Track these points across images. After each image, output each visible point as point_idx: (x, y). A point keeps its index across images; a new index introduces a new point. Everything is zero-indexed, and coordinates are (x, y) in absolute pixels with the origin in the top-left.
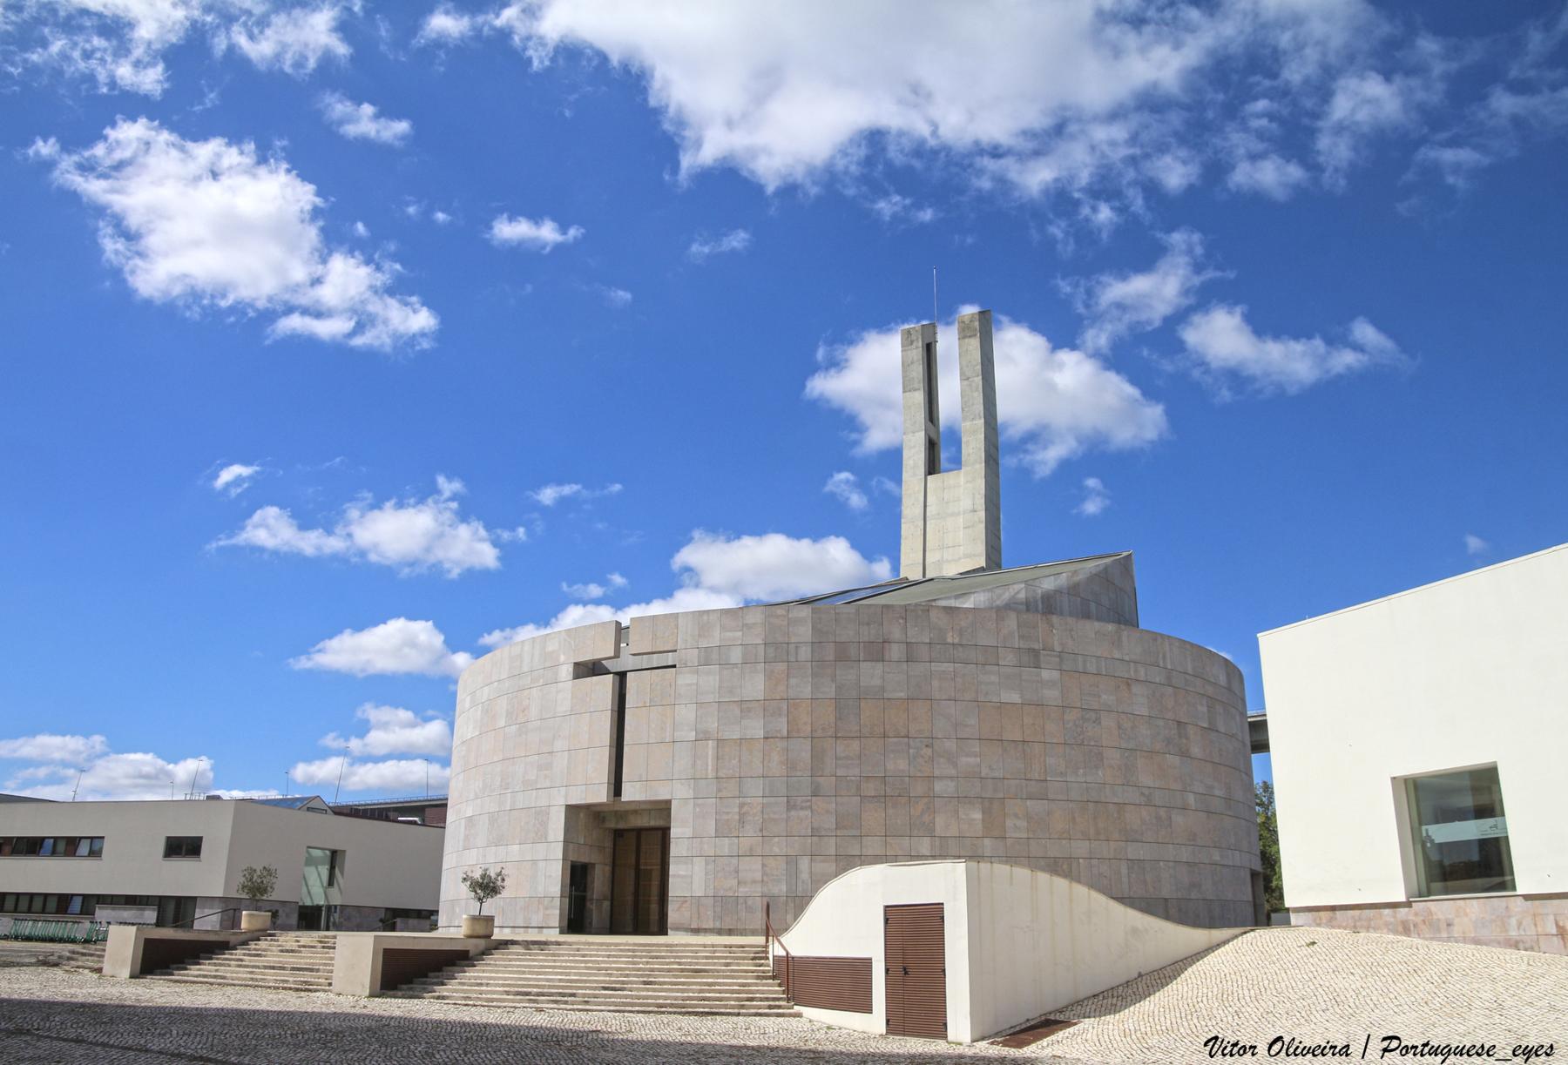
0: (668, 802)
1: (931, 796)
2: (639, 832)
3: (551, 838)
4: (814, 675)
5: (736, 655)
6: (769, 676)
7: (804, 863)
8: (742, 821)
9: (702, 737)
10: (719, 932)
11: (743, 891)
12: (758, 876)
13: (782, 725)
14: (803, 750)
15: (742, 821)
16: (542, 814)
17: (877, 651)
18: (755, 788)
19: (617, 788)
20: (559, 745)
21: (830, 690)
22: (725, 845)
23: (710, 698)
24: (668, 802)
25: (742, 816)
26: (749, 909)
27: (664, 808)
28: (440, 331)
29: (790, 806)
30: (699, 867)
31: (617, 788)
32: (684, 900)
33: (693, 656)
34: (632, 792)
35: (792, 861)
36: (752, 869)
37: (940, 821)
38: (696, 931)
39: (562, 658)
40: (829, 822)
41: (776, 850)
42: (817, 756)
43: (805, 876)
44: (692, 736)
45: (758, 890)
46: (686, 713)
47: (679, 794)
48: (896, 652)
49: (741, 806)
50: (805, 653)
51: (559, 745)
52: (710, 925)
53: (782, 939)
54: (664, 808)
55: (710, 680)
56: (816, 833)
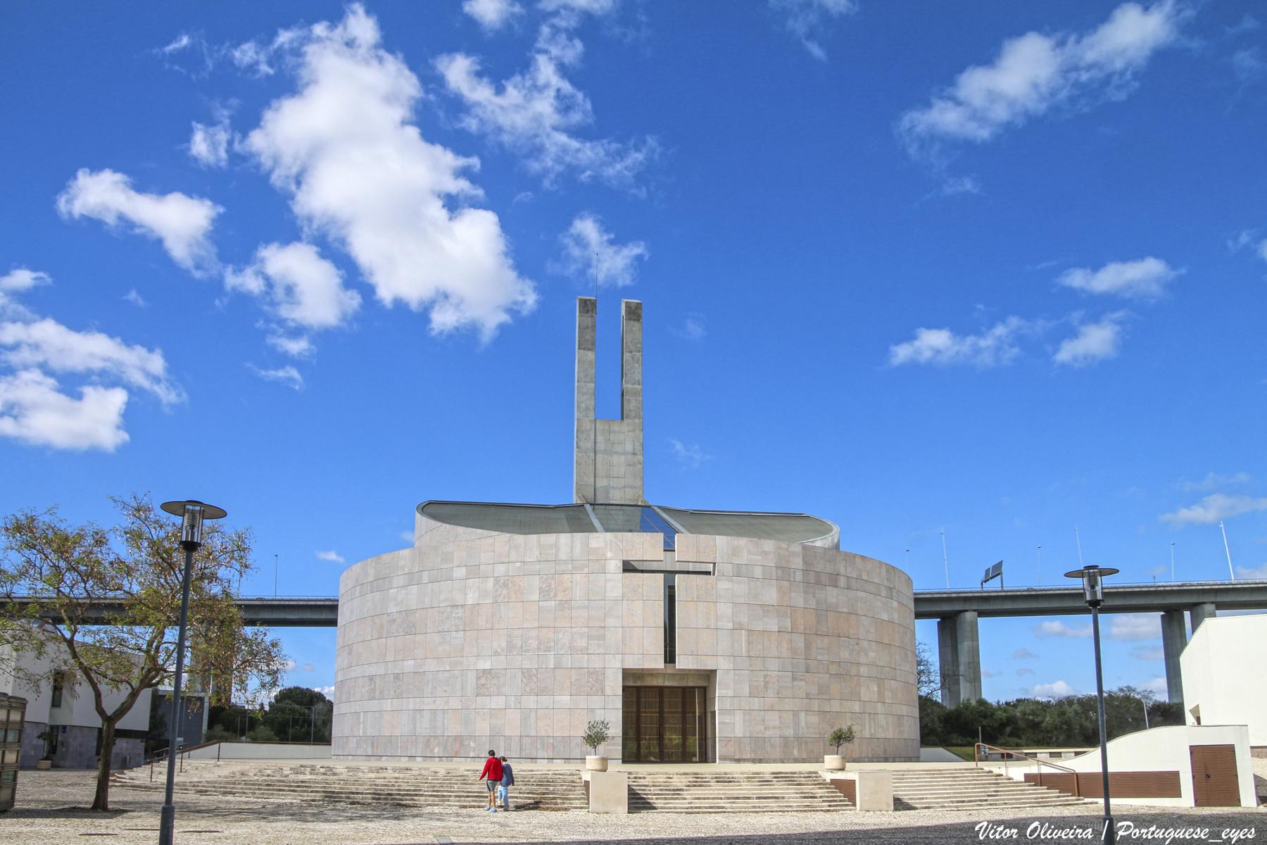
0: (714, 671)
1: (858, 676)
2: (661, 689)
3: (608, 691)
4: (805, 592)
5: (758, 572)
6: (780, 589)
7: (802, 715)
8: (766, 687)
9: (738, 627)
10: (754, 761)
11: (768, 734)
12: (777, 724)
13: (788, 624)
14: (800, 642)
15: (766, 687)
16: (597, 677)
17: (834, 580)
18: (774, 665)
19: (670, 657)
20: (611, 622)
21: (812, 604)
22: (756, 703)
23: (742, 601)
24: (714, 671)
25: (766, 683)
26: (772, 746)
27: (710, 675)
28: (952, 330)
29: (794, 679)
30: (739, 718)
31: (670, 657)
32: (728, 740)
33: (728, 569)
34: (1110, 686)
35: (795, 714)
36: (773, 719)
37: (863, 690)
38: (738, 761)
39: (609, 555)
40: (814, 690)
41: (787, 708)
42: (808, 646)
43: (803, 724)
44: (730, 626)
45: (777, 733)
46: (725, 609)
47: (722, 665)
48: (842, 582)
49: (766, 676)
50: (799, 576)
51: (611, 622)
52: (748, 756)
53: (1099, 769)
54: (710, 675)
55: (741, 588)
56: (808, 696)
